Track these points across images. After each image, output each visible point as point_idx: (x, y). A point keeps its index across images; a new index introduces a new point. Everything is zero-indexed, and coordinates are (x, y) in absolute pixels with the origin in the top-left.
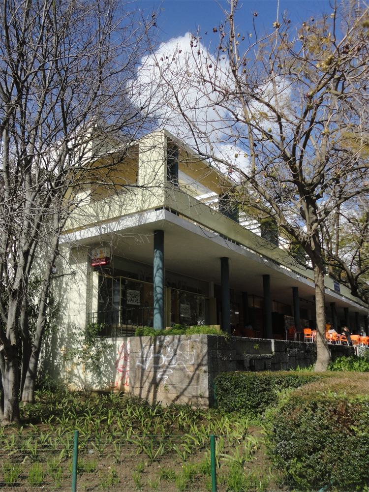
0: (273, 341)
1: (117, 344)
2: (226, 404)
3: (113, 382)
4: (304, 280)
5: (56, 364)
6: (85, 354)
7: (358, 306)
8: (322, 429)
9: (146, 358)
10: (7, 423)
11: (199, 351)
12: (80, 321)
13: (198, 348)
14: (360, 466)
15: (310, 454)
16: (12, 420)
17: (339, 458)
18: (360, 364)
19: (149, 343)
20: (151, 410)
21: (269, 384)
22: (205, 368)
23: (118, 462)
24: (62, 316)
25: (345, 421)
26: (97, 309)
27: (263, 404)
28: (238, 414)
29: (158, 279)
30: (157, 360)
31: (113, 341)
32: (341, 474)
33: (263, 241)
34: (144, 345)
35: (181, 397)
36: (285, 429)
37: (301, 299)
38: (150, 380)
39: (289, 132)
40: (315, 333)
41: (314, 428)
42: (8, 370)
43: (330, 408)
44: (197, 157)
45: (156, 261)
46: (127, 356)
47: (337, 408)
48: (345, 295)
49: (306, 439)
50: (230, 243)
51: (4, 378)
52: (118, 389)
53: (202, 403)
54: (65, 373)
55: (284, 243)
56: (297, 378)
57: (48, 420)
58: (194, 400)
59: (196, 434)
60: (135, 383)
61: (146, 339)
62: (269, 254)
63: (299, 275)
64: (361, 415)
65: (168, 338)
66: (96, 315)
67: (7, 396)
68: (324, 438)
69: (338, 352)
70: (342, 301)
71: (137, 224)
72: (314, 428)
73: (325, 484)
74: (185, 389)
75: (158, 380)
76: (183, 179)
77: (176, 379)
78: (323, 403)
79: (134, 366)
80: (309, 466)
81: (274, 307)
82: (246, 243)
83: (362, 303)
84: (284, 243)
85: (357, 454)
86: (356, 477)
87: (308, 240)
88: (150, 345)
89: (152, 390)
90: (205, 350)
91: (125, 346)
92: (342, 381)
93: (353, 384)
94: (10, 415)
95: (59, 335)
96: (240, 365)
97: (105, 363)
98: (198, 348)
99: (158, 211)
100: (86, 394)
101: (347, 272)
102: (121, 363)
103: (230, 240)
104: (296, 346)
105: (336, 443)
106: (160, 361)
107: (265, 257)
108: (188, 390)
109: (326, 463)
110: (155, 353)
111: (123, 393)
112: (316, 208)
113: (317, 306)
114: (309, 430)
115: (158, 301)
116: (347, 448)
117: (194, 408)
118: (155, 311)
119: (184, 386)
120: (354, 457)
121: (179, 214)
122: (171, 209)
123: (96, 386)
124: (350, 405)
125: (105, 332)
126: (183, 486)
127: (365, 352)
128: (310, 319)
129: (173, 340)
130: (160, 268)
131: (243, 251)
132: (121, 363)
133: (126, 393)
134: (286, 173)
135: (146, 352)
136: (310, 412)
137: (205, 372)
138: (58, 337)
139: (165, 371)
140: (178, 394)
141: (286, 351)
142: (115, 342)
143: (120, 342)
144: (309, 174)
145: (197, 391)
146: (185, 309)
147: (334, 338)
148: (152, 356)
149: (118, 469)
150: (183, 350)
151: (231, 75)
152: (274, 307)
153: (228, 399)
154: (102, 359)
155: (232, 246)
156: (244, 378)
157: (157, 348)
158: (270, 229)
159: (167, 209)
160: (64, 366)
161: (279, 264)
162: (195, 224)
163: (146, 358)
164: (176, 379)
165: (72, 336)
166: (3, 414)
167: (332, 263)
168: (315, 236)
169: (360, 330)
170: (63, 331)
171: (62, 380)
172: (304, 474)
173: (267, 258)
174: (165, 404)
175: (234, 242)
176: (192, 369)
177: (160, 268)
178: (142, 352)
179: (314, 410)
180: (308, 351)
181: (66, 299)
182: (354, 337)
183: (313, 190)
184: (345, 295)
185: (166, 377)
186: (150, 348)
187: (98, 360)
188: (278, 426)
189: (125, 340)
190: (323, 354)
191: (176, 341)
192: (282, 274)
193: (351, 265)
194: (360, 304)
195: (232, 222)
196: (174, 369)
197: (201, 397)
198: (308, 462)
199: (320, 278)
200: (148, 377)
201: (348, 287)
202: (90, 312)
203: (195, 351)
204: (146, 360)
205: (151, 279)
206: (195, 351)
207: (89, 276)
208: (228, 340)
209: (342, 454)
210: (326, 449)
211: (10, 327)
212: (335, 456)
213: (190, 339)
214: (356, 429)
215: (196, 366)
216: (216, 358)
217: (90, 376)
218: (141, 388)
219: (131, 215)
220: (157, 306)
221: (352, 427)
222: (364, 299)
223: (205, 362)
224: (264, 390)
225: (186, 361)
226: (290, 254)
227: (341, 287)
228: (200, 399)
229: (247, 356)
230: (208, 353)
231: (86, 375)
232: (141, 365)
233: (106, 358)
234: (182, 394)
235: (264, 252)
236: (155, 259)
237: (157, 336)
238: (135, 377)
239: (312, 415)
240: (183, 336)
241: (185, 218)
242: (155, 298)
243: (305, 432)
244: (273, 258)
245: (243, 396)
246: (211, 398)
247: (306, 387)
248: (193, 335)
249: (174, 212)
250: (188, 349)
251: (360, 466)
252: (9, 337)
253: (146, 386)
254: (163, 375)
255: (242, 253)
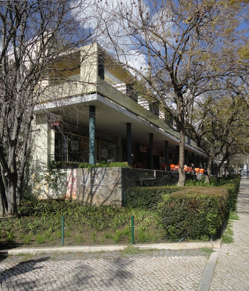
0: (155, 171)
1: (68, 173)
2: (133, 204)
3: (65, 194)
4: (172, 137)
5: (29, 185)
6: (48, 179)
7: (199, 152)
8: (184, 211)
9: (86, 180)
10: (11, 216)
11: (117, 176)
12: (44, 159)
13: (116, 175)
14: (200, 227)
15: (178, 223)
16: (14, 214)
17: (191, 224)
18: (199, 183)
19: (88, 172)
20: (90, 209)
21: (155, 193)
22: (120, 186)
23: (81, 232)
24: (32, 156)
25: (194, 207)
26: (54, 152)
27: (152, 203)
28: (139, 209)
29: (92, 135)
30: (92, 181)
31: (65, 171)
32: (191, 231)
33: (150, 114)
34: (85, 173)
35: (107, 201)
36: (167, 211)
37: (169, 148)
38: (89, 193)
39: (171, 52)
40: (177, 167)
41: (181, 211)
42: (10, 187)
43: (188, 201)
44: (118, 64)
45: (91, 124)
46: (74, 179)
47: (191, 201)
48: (193, 146)
49: (177, 216)
50: (133, 115)
51: (7, 192)
52: (68, 198)
53: (118, 204)
54: (35, 190)
55: (162, 115)
56: (170, 189)
57: (34, 214)
58: (114, 202)
59: (118, 219)
60: (79, 194)
61: (86, 170)
62: (154, 122)
63: (153, 125)
64: (202, 204)
65: (99, 169)
66: (54, 156)
67: (10, 201)
68: (185, 215)
69: (190, 177)
70: (191, 149)
71: (80, 102)
72: (181, 211)
73: (184, 236)
74: (109, 197)
75: (93, 193)
76: (107, 76)
77: (103, 192)
78: (185, 199)
79: (79, 185)
80: (177, 228)
81: (154, 152)
82: (142, 115)
83: (202, 150)
84: (162, 115)
85: (199, 222)
86: (198, 232)
87: (178, 116)
88: (89, 173)
89: (90, 198)
90: (120, 176)
91: (72, 174)
92: (193, 190)
93: (198, 191)
94: (12, 212)
95: (30, 167)
96: (138, 183)
97: (60, 183)
98: (116, 175)
99: (93, 95)
100: (50, 200)
101: (196, 133)
102: (70, 183)
103: (133, 113)
104: (166, 174)
105: (190, 217)
106: (94, 182)
107: (151, 123)
108: (110, 197)
109: (185, 226)
110: (91, 177)
111: (71, 200)
112: (182, 99)
113: (180, 152)
114: (178, 212)
115: (92, 148)
116: (195, 219)
117: (114, 207)
118: (90, 154)
119: (108, 195)
120: (198, 223)
121: (104, 96)
122: (101, 93)
123: (55, 197)
124: (197, 200)
125: (59, 167)
126: (117, 240)
127: (201, 177)
128: (173, 159)
129: (102, 170)
130: (94, 129)
131: (140, 119)
132: (70, 183)
133: (73, 200)
134: (167, 77)
135: (86, 177)
136: (179, 203)
137: (120, 187)
138: (30, 168)
139: (97, 188)
140: (105, 200)
141: (161, 176)
142: (66, 172)
143: (69, 171)
144: (180, 78)
145: (115, 198)
146: (104, 153)
147: (186, 170)
148: (89, 179)
149: (82, 235)
150: (108, 175)
151: (140, 17)
152: (154, 152)
153: (135, 202)
154: (58, 181)
155: (134, 117)
156: (143, 190)
157: (93, 175)
158: (155, 107)
159: (98, 93)
160: (34, 186)
161: (159, 127)
162: (112, 102)
163: (86, 180)
164: (104, 191)
165: (38, 168)
166: (8, 211)
167: (188, 128)
168: (182, 113)
169: (199, 165)
170: (33, 165)
171: (33, 195)
172: (175, 231)
173: (153, 124)
174: (98, 205)
175: (135, 114)
176: (113, 186)
177: (94, 129)
178: (84, 177)
179: (180, 202)
180: (173, 177)
181: (34, 145)
182: (197, 169)
183: (182, 88)
184: (193, 146)
185: (98, 191)
186: (88, 174)
187: (56, 181)
188: (164, 210)
189: (72, 170)
190: (182, 178)
191: (104, 171)
192: (160, 133)
193: (198, 129)
194: (200, 151)
195: (134, 102)
196: (102, 186)
197: (118, 201)
198: (177, 226)
199: (183, 137)
200: (87, 191)
201: (195, 141)
202: (50, 154)
203: (114, 176)
204: (86, 181)
205: (88, 135)
206: (114, 176)
207: (49, 132)
208: (132, 170)
209: (192, 222)
210: (185, 220)
211: (10, 162)
212: (189, 223)
213: (112, 169)
214: (199, 211)
215: (115, 185)
216: (126, 180)
217: (51, 192)
218: (83, 197)
219: (76, 96)
220: (91, 151)
221: (197, 210)
222: (203, 148)
223: (120, 182)
224: (153, 196)
225: (109, 182)
226: (165, 122)
227: (191, 141)
228: (117, 202)
229: (142, 179)
230: (122, 177)
231: (49, 190)
232: (83, 184)
233: (61, 180)
234: (107, 199)
235: (151, 120)
236: (90, 123)
237: (92, 168)
238: (80, 191)
239: (180, 205)
240: (108, 168)
241: (108, 99)
242: (90, 146)
243: (176, 212)
244: (156, 124)
245: (141, 199)
246: (123, 201)
247: (176, 193)
248: (113, 168)
249: (102, 95)
250: (110, 175)
251: (200, 227)
252: (10, 168)
253: (86, 195)
254: (96, 189)
255: (139, 120)
